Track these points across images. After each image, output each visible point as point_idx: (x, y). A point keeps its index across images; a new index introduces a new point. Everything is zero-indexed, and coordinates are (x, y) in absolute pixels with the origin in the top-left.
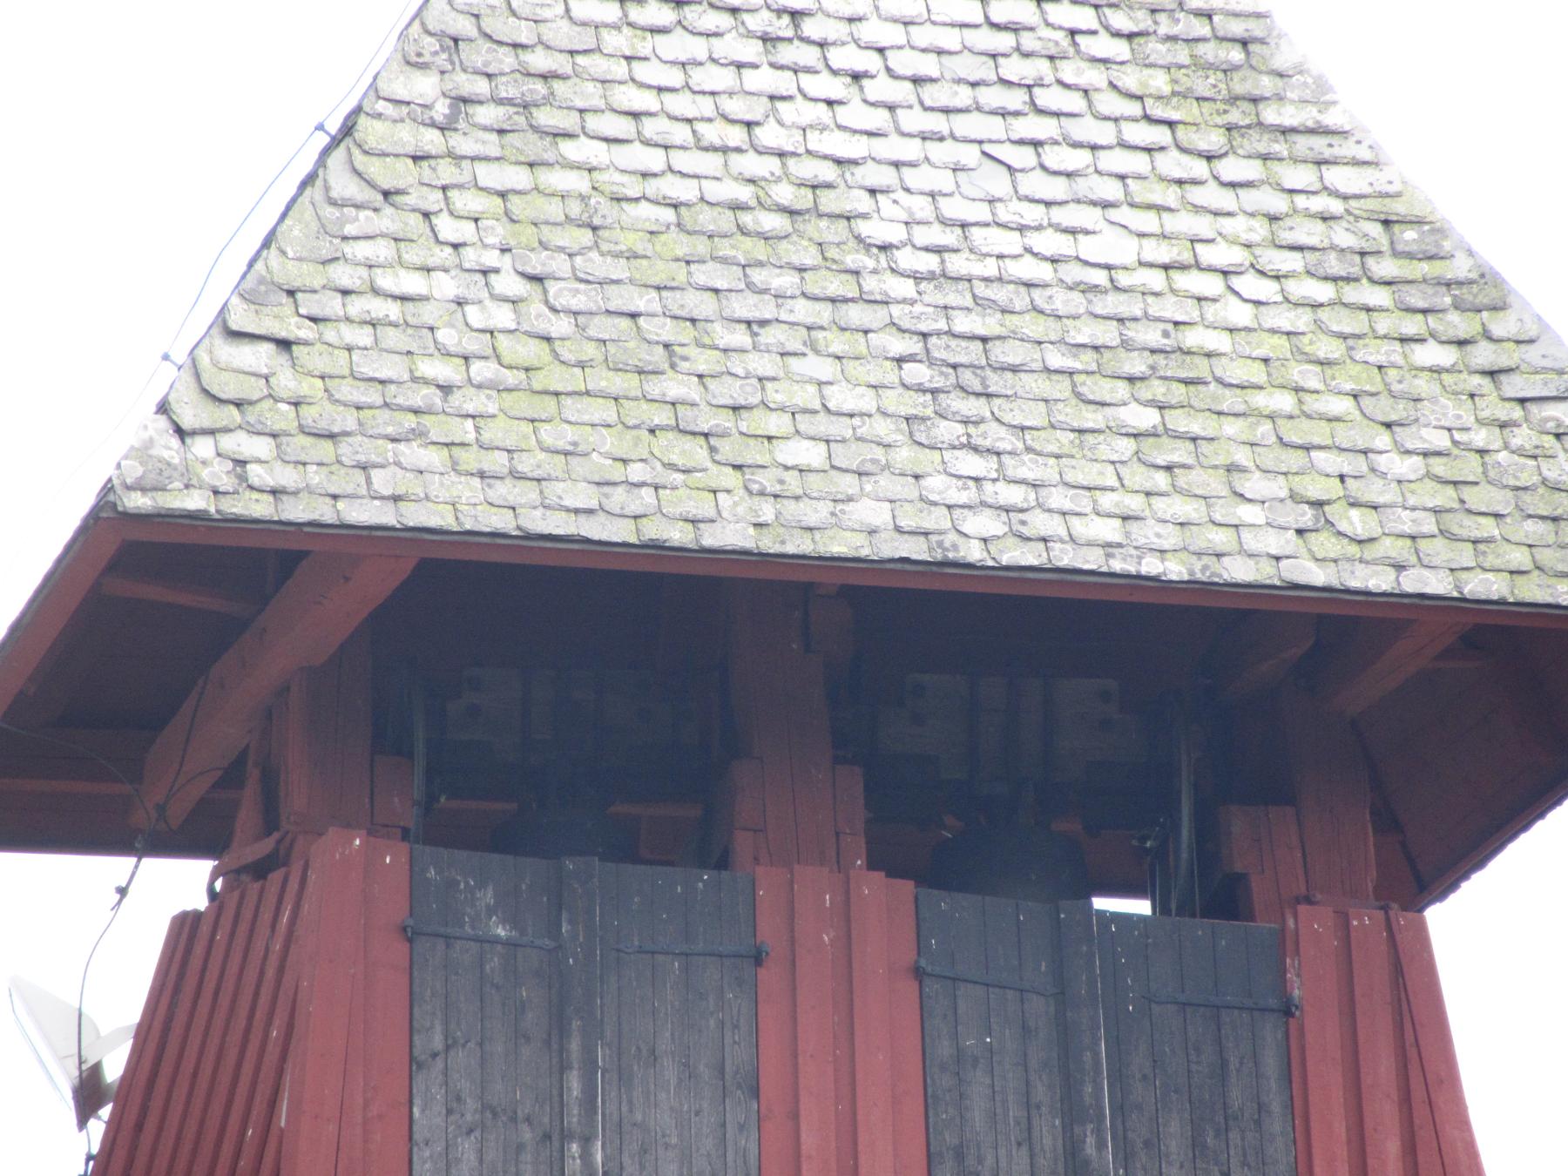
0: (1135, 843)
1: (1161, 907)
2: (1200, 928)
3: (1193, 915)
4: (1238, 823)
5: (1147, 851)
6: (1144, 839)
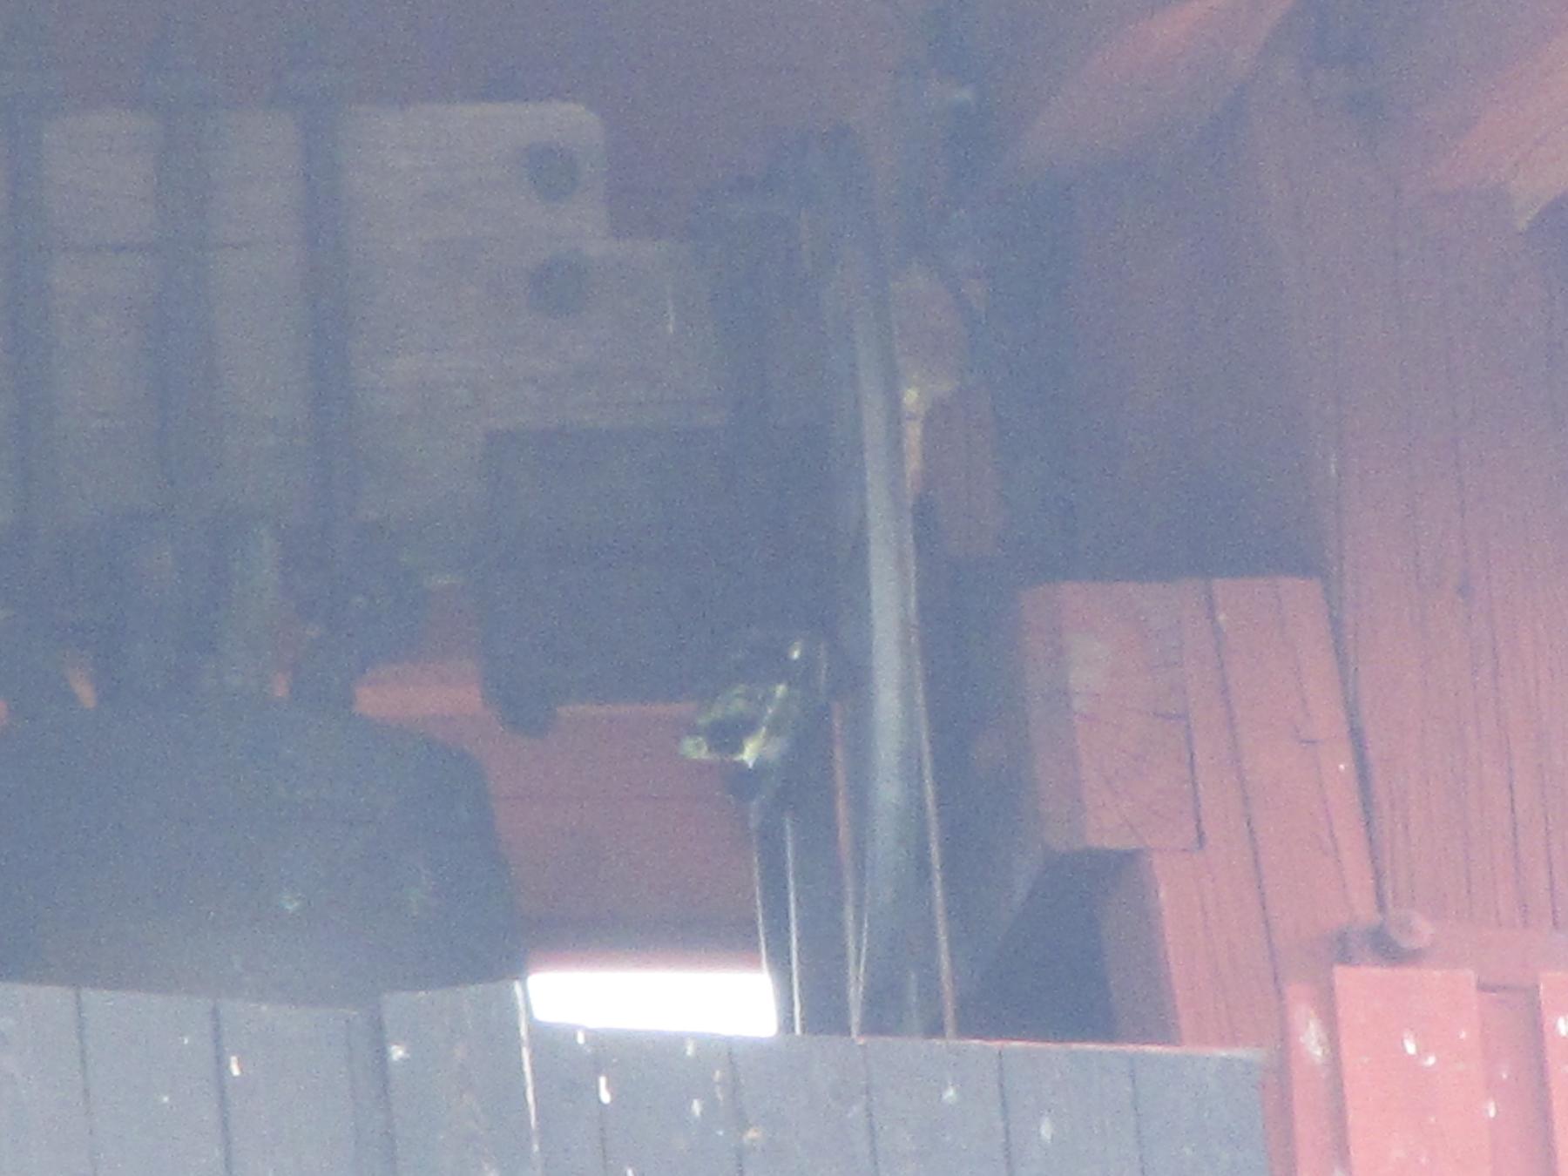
0: (696, 750)
1: (819, 1007)
2: (952, 1076)
3: (935, 1029)
4: (1095, 651)
5: (743, 781)
6: (728, 735)
